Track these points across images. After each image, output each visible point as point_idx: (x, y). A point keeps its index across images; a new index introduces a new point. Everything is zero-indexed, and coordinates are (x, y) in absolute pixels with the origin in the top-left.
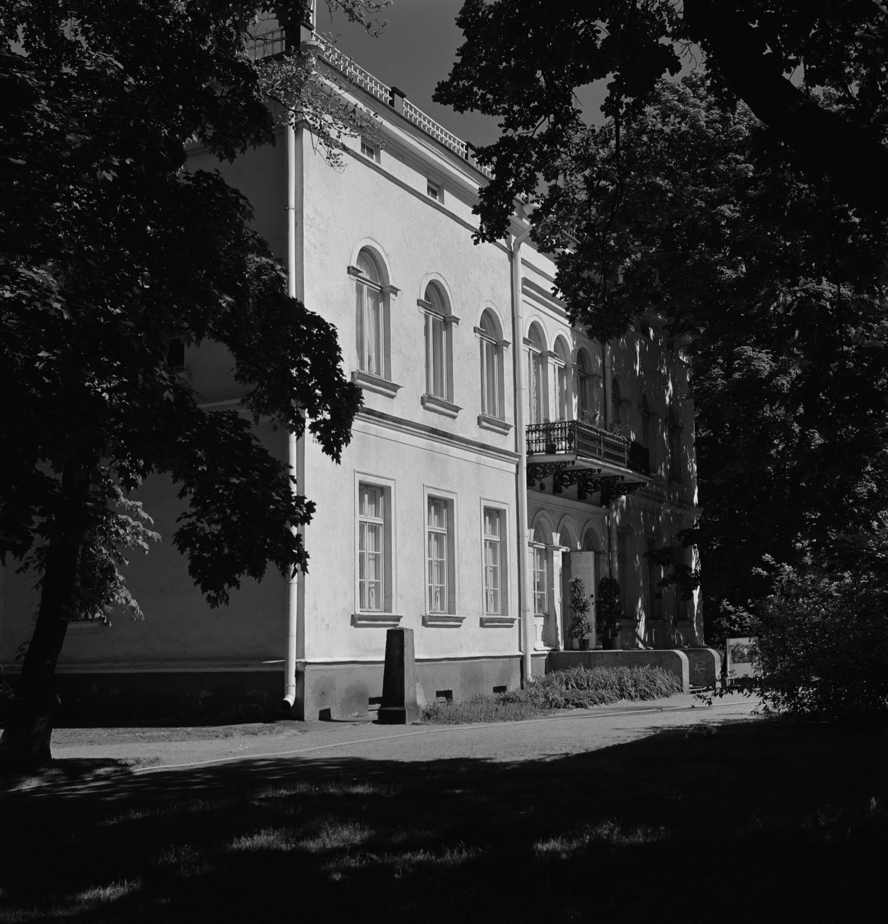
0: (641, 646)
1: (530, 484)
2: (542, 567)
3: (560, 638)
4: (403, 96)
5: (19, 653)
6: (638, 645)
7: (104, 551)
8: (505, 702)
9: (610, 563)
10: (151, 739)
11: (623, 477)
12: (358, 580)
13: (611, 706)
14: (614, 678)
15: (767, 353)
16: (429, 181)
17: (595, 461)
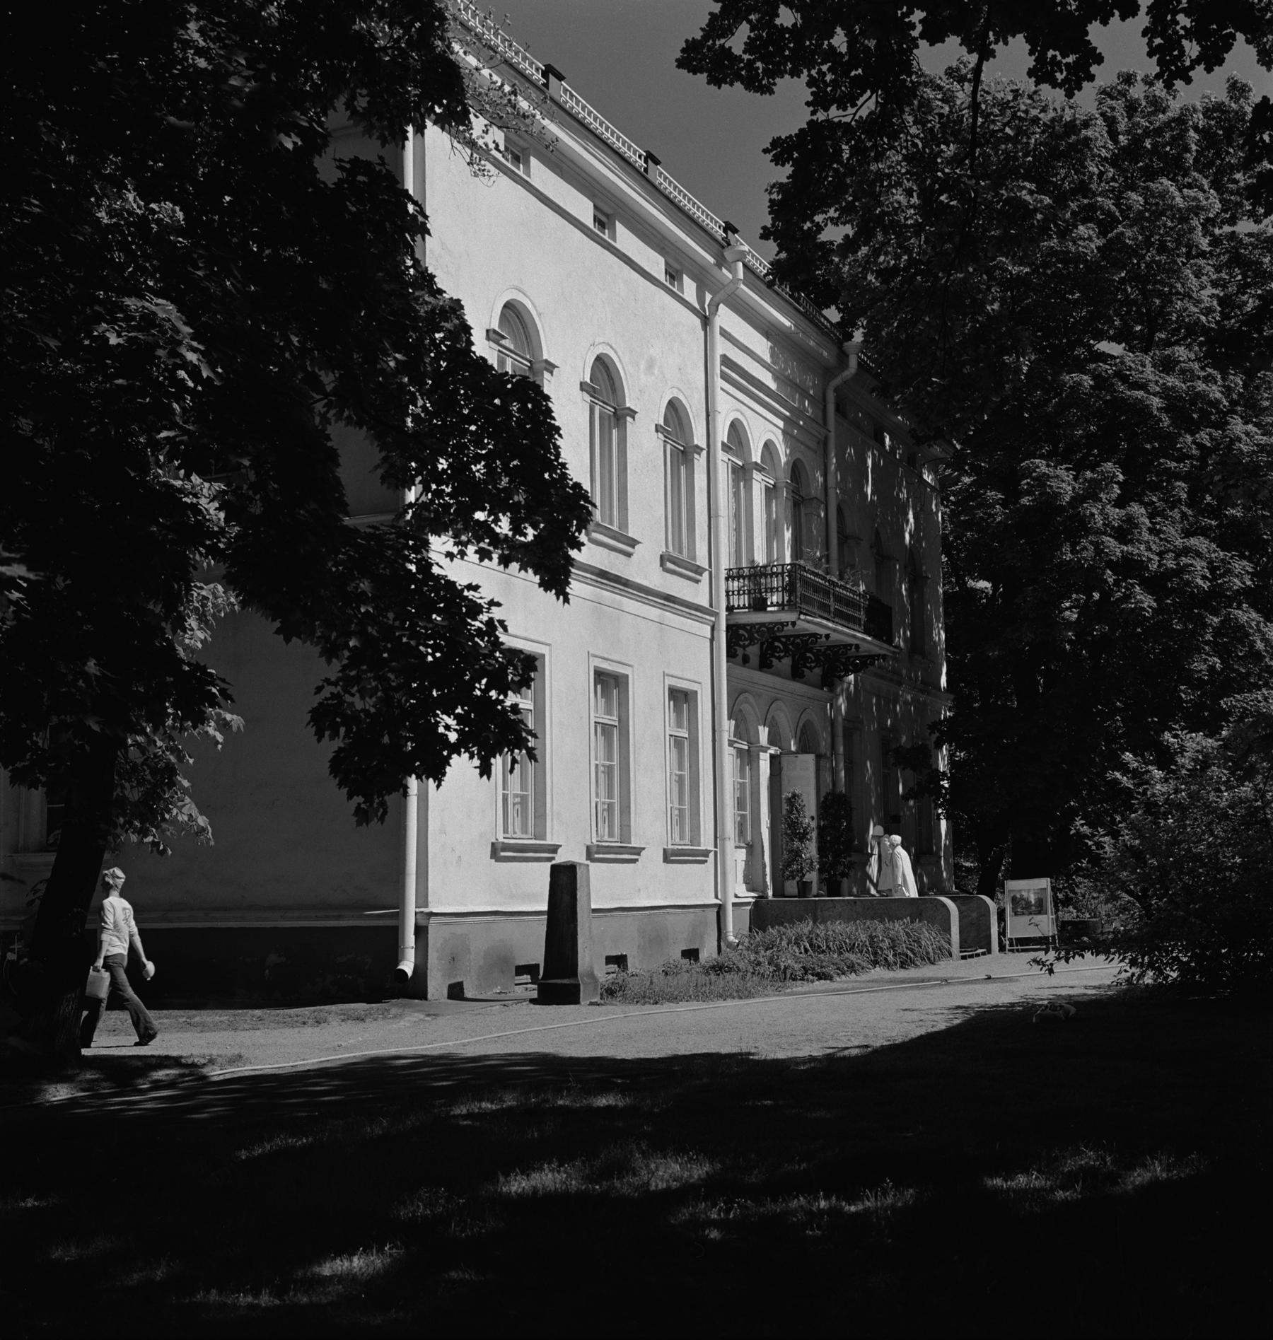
0: (873, 891)
1: (731, 655)
2: (743, 776)
3: (768, 879)
4: (560, 78)
5: (31, 897)
6: (869, 890)
7: (159, 743)
8: (714, 974)
9: (834, 772)
10: (204, 1028)
11: (857, 647)
12: (500, 791)
13: (864, 977)
14: (863, 937)
15: (1067, 469)
16: (596, 207)
17: (824, 622)
